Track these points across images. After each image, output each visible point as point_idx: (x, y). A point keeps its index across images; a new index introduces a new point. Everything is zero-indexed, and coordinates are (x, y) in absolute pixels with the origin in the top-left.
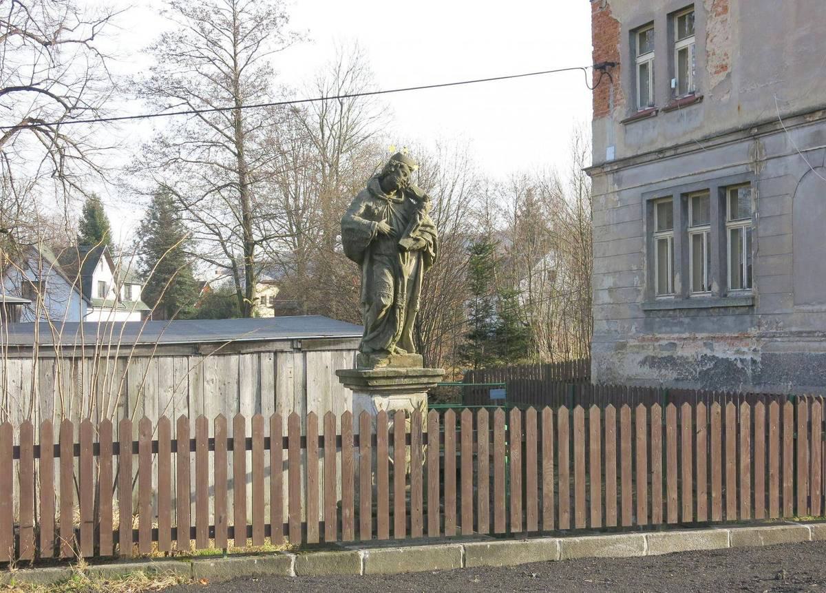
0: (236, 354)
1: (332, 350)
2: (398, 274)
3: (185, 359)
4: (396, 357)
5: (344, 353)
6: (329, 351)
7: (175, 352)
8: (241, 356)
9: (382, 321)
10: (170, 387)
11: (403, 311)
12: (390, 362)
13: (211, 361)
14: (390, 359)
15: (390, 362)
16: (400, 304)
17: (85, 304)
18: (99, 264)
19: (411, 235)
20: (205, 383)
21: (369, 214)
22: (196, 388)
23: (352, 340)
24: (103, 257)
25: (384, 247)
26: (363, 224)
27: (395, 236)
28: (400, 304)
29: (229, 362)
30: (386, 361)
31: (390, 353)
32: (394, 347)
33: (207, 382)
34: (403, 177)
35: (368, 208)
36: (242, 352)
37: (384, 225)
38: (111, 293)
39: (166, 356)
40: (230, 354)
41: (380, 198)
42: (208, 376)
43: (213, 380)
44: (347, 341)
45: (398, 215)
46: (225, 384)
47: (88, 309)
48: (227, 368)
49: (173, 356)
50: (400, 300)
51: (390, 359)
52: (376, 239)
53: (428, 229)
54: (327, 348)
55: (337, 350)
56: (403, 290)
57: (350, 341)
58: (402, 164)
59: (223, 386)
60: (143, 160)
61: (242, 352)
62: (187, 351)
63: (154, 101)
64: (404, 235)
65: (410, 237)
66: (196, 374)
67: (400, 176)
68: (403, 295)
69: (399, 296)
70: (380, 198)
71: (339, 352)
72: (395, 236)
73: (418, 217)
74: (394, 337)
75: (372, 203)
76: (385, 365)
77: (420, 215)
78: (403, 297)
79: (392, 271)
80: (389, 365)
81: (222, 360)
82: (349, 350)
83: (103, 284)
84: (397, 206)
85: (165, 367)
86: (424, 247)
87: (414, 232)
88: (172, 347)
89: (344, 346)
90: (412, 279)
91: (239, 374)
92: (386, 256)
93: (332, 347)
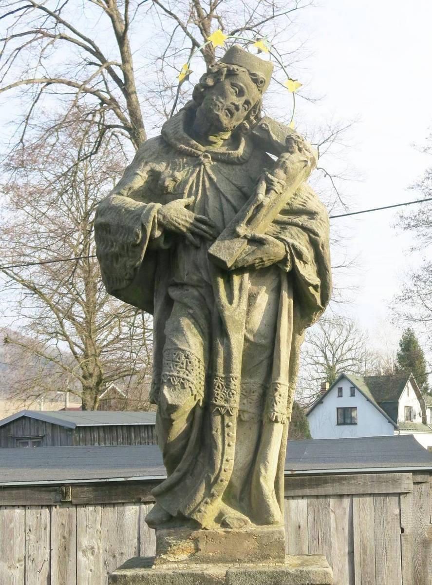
0: (135, 503)
1: (308, 497)
2: (214, 329)
3: (45, 511)
4: (214, 537)
5: (332, 501)
6: (303, 497)
7: (27, 499)
8: (143, 506)
9: (184, 447)
10: (19, 561)
11: (233, 422)
12: (197, 549)
13: (89, 515)
14: (196, 541)
15: (197, 549)
16: (222, 403)
17: (393, 427)
18: (405, 390)
19: (242, 230)
20: (80, 553)
21: (156, 191)
22: (63, 561)
23: (345, 479)
24: (409, 384)
25: (187, 267)
26: (128, 211)
27: (204, 233)
28: (220, 402)
29: (121, 516)
30: (189, 545)
31: (197, 525)
32: (218, 504)
33: (84, 551)
34: (234, 99)
35: (155, 176)
36: (143, 499)
37: (179, 213)
38: (417, 416)
39: (13, 506)
40: (123, 504)
41: (182, 153)
42: (85, 542)
43: (92, 548)
44: (334, 481)
45: (224, 187)
46: (114, 556)
47: (395, 432)
48: (120, 527)
49: (24, 506)
50: (219, 393)
51: (196, 541)
52: (163, 246)
53: (302, 220)
54: (300, 492)
55: (317, 497)
56: (228, 368)
57: (340, 480)
58: (233, 67)
59: (111, 559)
60: (415, 289)
61: (143, 499)
62: (51, 496)
63: (424, 233)
64: (224, 233)
65: (238, 236)
66: (64, 538)
67: (223, 94)
68: (228, 379)
69: (219, 382)
70: (182, 153)
71: (321, 500)
72: (204, 233)
73: (263, 186)
74: (209, 486)
75: (165, 164)
76: (184, 556)
77: (270, 183)
78: (228, 386)
79: (202, 321)
80: (195, 557)
81: (110, 513)
82: (341, 496)
83: (409, 409)
84: (225, 170)
85: (12, 525)
86: (284, 261)
87: (249, 222)
88: (21, 491)
89: (329, 489)
90: (263, 341)
91: (139, 539)
92: (193, 286)
93: (307, 491)
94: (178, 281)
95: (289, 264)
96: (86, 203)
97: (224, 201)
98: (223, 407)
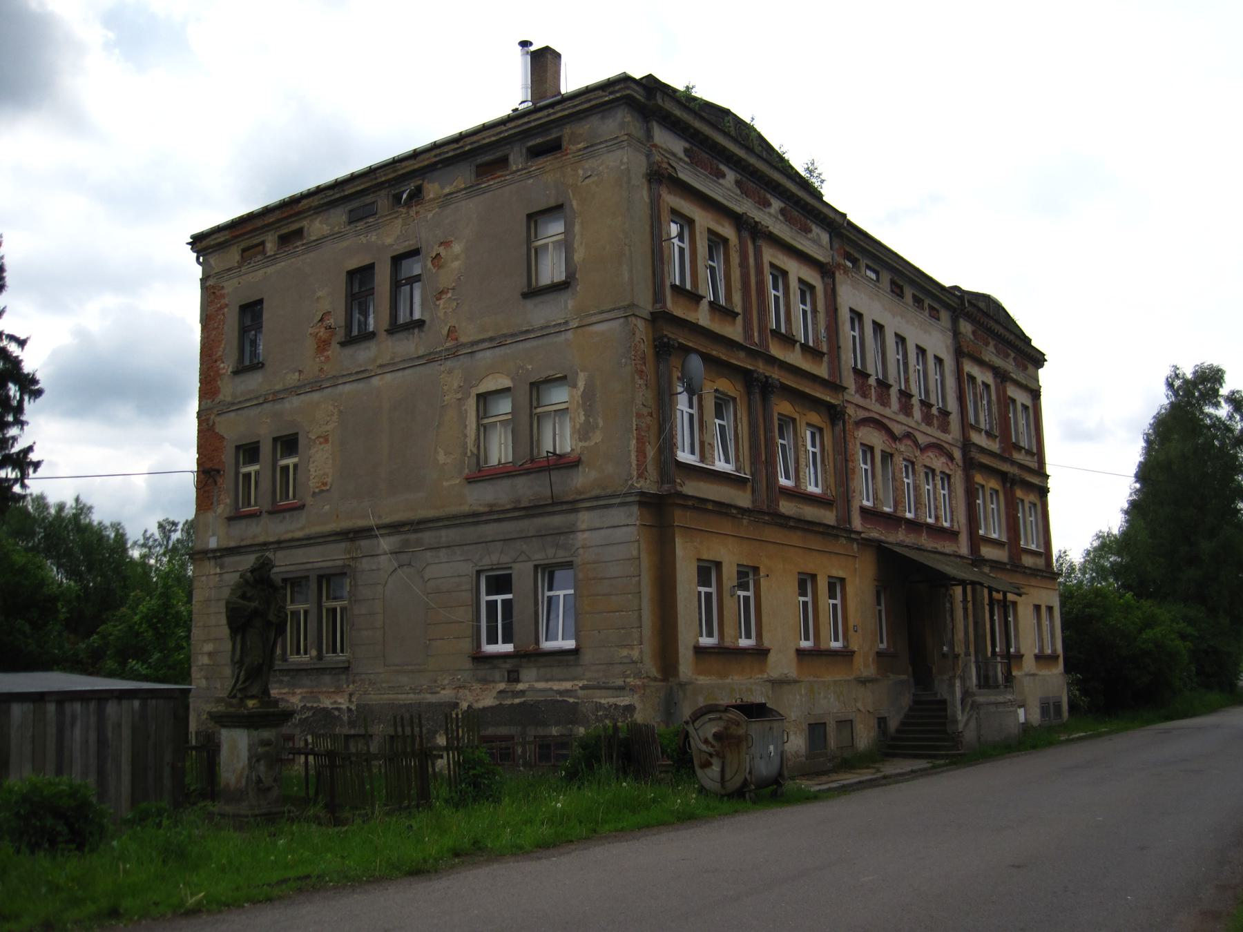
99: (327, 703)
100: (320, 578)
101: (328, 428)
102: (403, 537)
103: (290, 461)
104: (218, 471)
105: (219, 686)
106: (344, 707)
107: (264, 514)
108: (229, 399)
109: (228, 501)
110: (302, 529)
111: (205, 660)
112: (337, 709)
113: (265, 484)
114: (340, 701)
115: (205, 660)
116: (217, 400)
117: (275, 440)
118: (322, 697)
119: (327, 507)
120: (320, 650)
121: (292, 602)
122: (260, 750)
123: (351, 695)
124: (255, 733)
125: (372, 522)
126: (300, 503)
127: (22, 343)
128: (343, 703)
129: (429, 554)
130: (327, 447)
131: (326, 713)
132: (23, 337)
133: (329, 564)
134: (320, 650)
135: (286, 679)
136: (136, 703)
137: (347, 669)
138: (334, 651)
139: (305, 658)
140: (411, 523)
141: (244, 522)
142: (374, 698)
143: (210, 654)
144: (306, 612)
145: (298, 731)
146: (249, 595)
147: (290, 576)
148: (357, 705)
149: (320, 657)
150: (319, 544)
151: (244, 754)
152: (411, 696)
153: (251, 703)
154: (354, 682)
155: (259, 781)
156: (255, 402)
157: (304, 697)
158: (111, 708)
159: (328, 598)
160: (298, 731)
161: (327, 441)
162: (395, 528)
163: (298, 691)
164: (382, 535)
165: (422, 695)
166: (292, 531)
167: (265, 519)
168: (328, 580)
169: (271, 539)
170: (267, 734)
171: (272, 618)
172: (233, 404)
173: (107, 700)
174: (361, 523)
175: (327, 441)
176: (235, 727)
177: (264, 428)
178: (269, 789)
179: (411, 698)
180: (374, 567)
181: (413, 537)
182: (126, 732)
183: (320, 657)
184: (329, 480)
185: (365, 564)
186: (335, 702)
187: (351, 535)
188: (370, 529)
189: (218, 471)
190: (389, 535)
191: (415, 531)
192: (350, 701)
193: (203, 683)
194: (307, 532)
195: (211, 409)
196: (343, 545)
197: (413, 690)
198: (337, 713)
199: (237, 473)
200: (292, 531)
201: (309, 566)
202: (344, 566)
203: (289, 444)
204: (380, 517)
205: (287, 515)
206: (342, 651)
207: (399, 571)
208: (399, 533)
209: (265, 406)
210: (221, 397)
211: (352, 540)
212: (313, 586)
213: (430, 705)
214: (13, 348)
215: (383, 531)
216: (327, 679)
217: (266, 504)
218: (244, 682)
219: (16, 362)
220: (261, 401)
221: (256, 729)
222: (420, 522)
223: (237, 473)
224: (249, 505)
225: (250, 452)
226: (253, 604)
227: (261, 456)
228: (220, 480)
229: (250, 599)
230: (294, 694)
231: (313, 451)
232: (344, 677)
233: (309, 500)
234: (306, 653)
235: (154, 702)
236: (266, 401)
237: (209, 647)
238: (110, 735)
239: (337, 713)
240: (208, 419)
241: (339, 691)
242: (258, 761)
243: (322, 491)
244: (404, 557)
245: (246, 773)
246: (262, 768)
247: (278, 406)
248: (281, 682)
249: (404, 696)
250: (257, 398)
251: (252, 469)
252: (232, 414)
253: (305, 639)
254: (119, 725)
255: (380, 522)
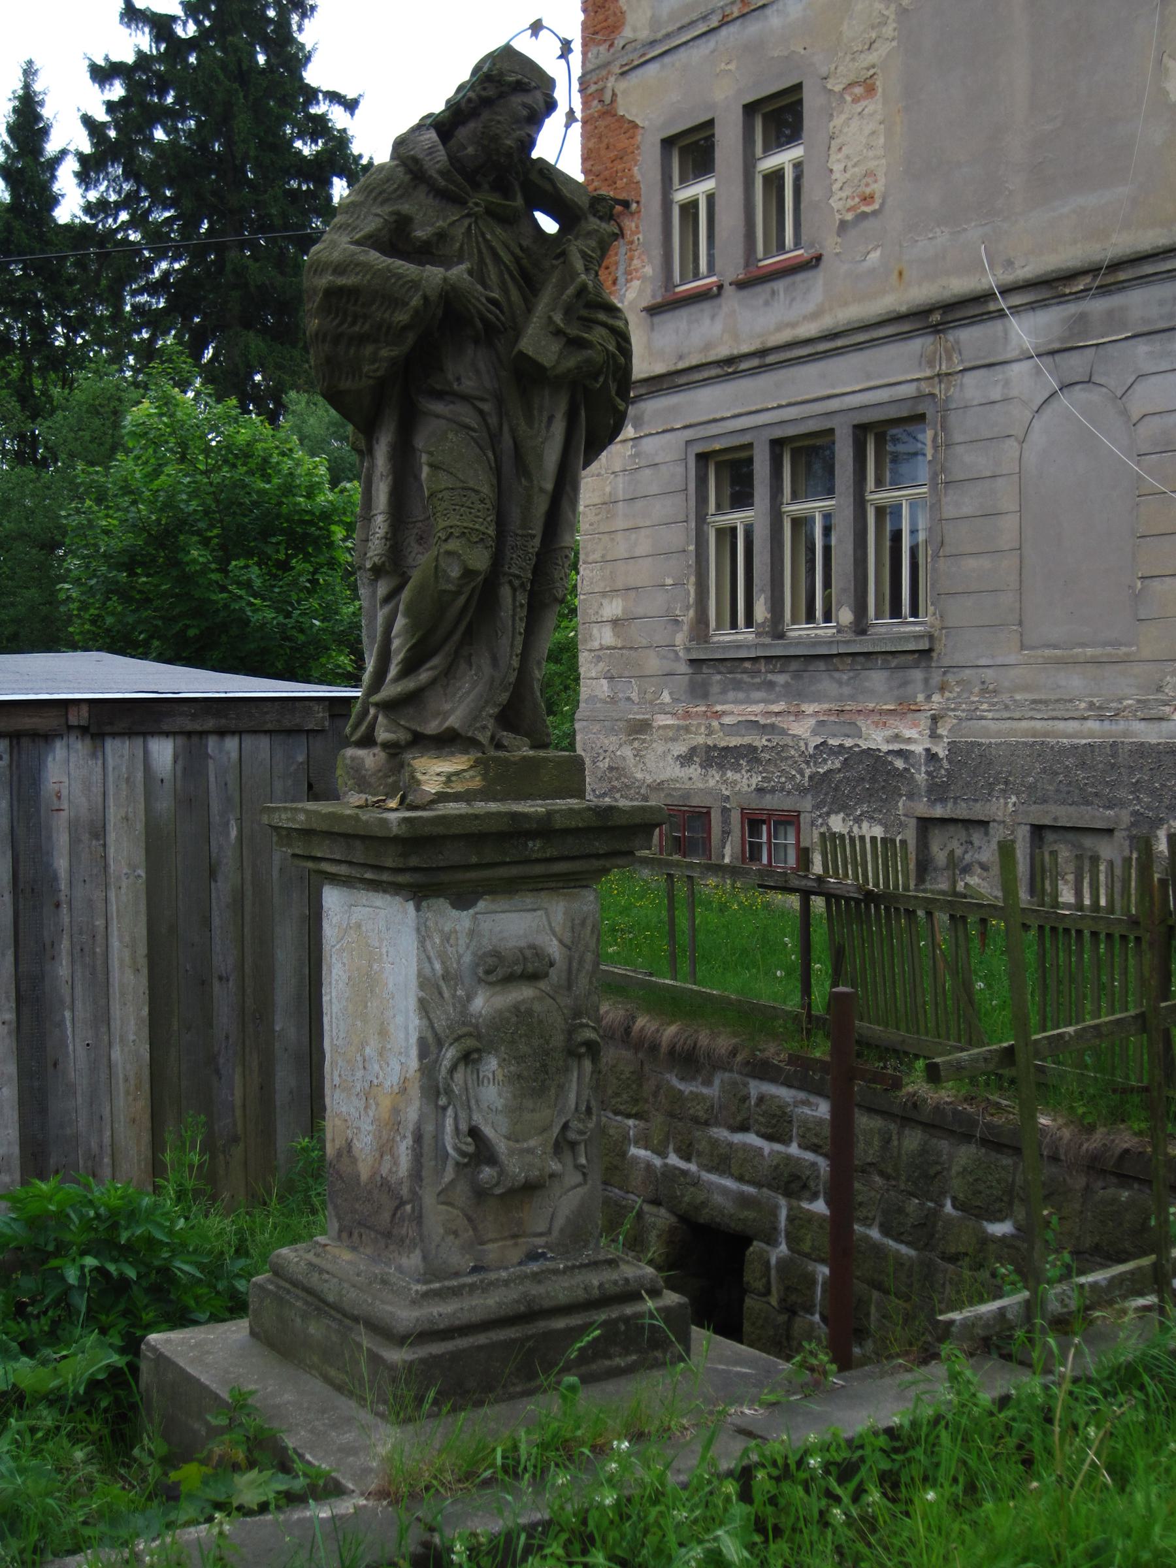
94: (438, 387)
95: (601, 379)
96: (480, 252)
97: (506, 276)
98: (518, 577)
99: (876, 739)
100: (861, 431)
101: (873, 57)
102: (1072, 309)
103: (784, 158)
104: (626, 204)
105: (634, 696)
106: (918, 749)
107: (729, 290)
108: (644, 34)
109: (648, 270)
110: (815, 316)
111: (606, 637)
112: (900, 753)
113: (730, 220)
114: (907, 733)
115: (606, 637)
116: (619, 43)
117: (750, 109)
118: (863, 724)
119: (875, 256)
120: (860, 609)
121: (795, 496)
122: (482, 1003)
123: (935, 719)
124: (458, 921)
125: (990, 280)
126: (812, 252)
127: (351, 106)
128: (915, 736)
129: (1142, 348)
130: (872, 106)
131: (875, 761)
132: (351, 96)
133: (883, 395)
134: (860, 609)
135: (781, 679)
136: (163, 751)
137: (926, 653)
138: (896, 612)
139: (823, 631)
140: (1093, 270)
141: (684, 314)
142: (995, 729)
143: (615, 622)
144: (827, 517)
145: (807, 804)
146: (421, 233)
147: (791, 431)
148: (953, 747)
149: (860, 627)
150: (858, 347)
151: (406, 1026)
152: (1092, 725)
153: (434, 772)
154: (942, 689)
155: (480, 1150)
156: (702, 28)
157: (821, 723)
158: (66, 769)
159: (879, 482)
160: (807, 804)
161: (871, 90)
162: (1050, 287)
163: (809, 708)
164: (1016, 310)
165: (1121, 725)
166: (793, 325)
167: (731, 300)
168: (886, 436)
169: (745, 348)
170: (521, 924)
171: (537, 342)
172: (653, 43)
173: (47, 738)
174: (960, 285)
175: (871, 90)
176: (375, 886)
177: (717, 83)
178: (530, 1188)
179: (1092, 730)
180: (996, 394)
181: (1097, 306)
182: (125, 853)
183: (860, 627)
184: (878, 188)
185: (972, 387)
186: (897, 737)
187: (936, 317)
188: (988, 296)
189: (626, 204)
190: (1032, 306)
191: (1105, 290)
192: (934, 736)
193: (603, 688)
194: (827, 323)
195: (607, 65)
196: (917, 345)
197: (1099, 712)
198: (899, 764)
199: (667, 203)
200: (793, 325)
201: (834, 405)
202: (919, 397)
203: (779, 115)
204: (1009, 263)
205: (780, 285)
206: (914, 613)
207: (1063, 399)
208: (1061, 299)
209: (724, 32)
210: (627, 33)
211: (937, 329)
212: (844, 453)
213: (1141, 750)
214: (338, 117)
215: (1017, 299)
216: (877, 679)
217: (731, 267)
218: (410, 667)
219: (341, 141)
220: (714, 22)
221: (462, 901)
222: (1115, 266)
223: (667, 203)
224: (696, 276)
225: (693, 149)
226: (434, 274)
227: (719, 155)
228: (629, 225)
229: (424, 253)
230: (799, 714)
231: (838, 121)
232: (917, 675)
233: (830, 245)
234: (827, 618)
235: (231, 743)
236: (724, 23)
237: (613, 608)
238: (61, 864)
239: (899, 764)
240: (602, 90)
241: (906, 709)
242: (468, 1058)
243: (864, 216)
244: (1075, 364)
245: (412, 1114)
246: (491, 1093)
247: (753, 28)
248: (771, 685)
249: (1072, 726)
250: (704, 18)
251: (700, 189)
252: (653, 68)
253: (827, 584)
254: (99, 832)
255: (1009, 278)
